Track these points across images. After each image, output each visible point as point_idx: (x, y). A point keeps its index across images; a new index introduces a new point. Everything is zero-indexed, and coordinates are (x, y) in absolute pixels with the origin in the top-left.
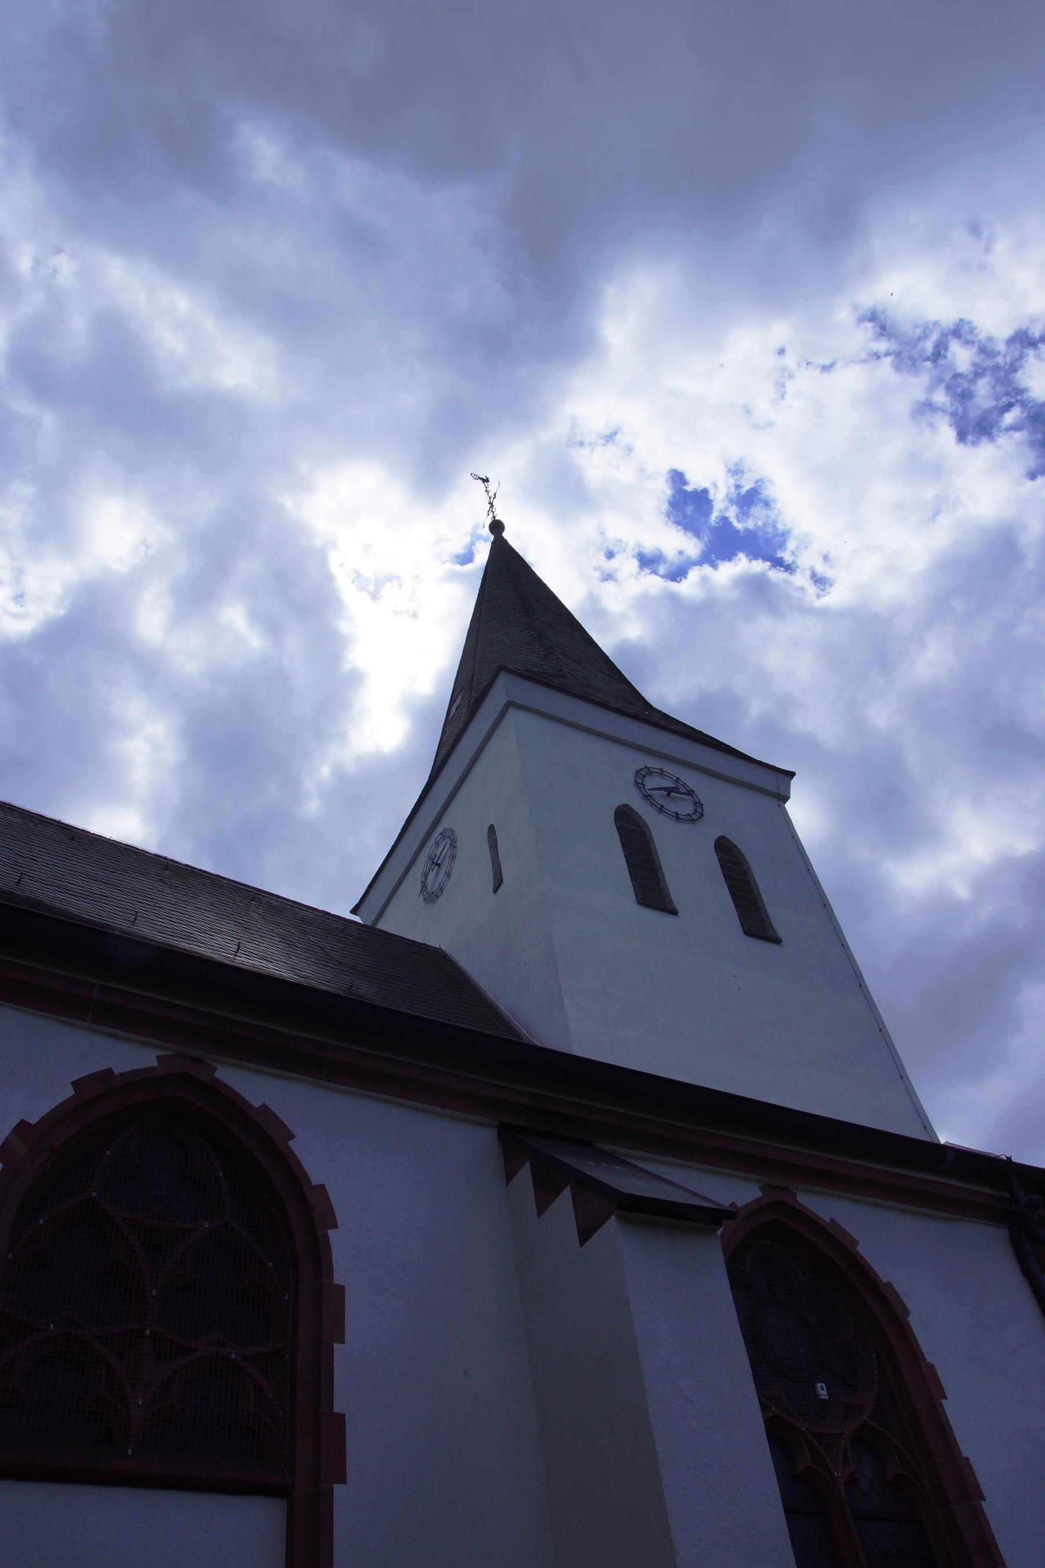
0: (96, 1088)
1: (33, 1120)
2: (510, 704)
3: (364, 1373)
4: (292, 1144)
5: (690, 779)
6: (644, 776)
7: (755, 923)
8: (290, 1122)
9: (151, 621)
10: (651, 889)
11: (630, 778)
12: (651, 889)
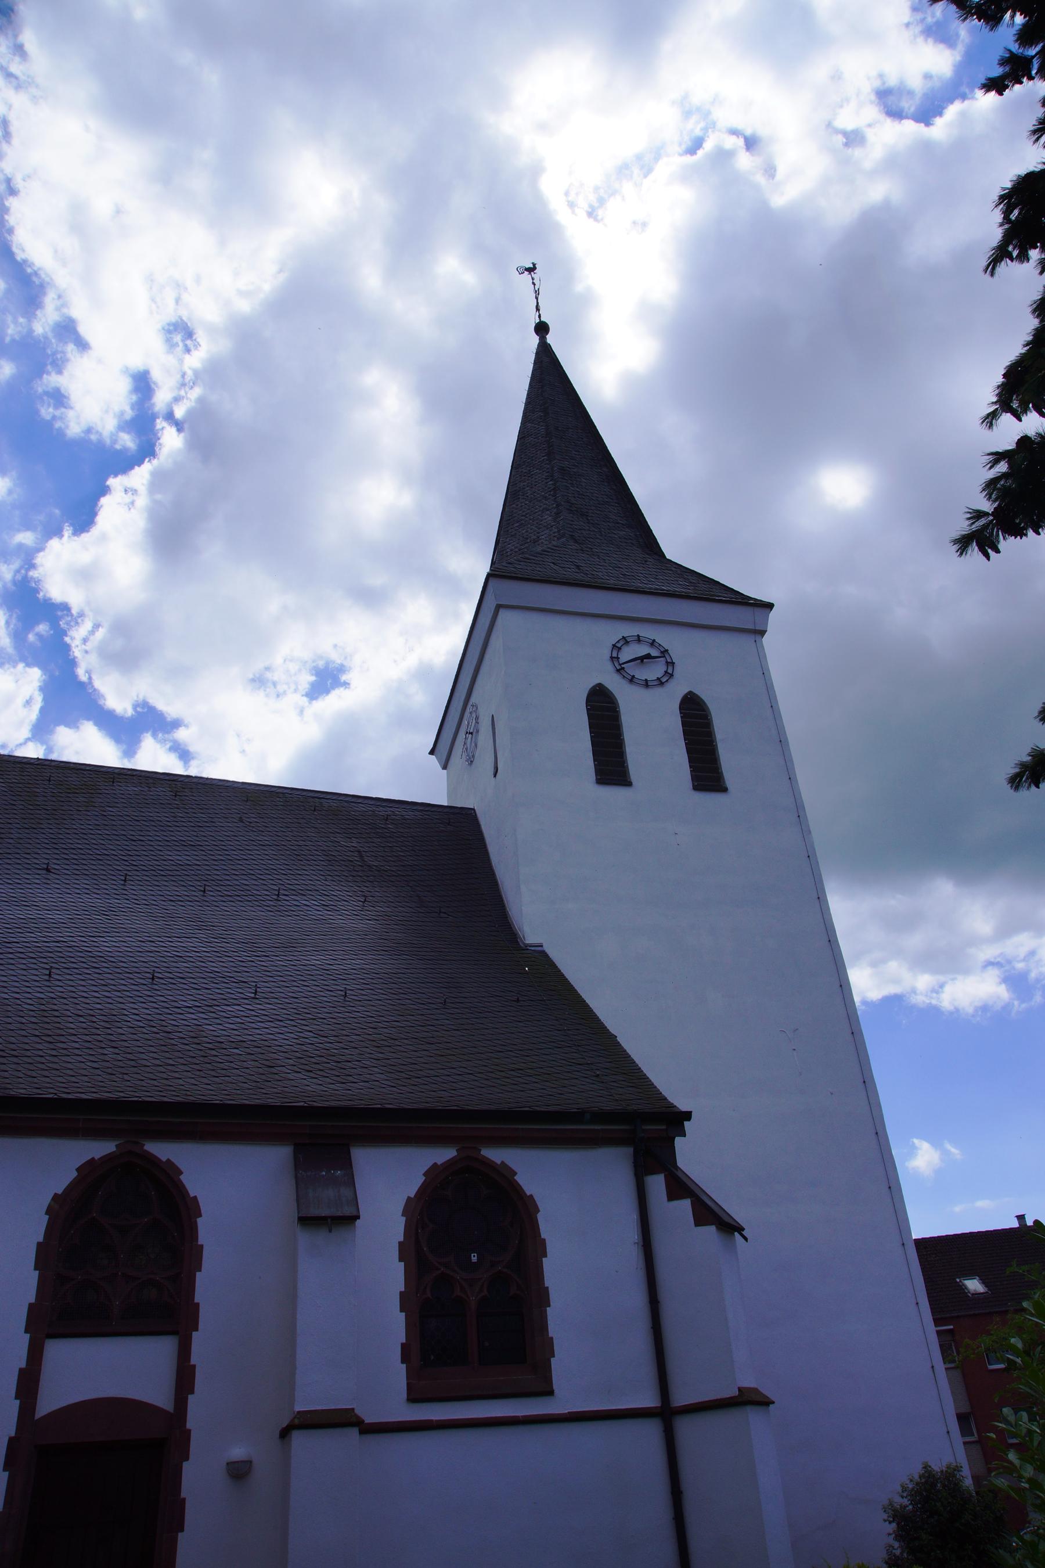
0: (88, 1169)
1: (60, 1192)
2: (499, 607)
3: (210, 1287)
4: (182, 1177)
5: (665, 637)
6: (620, 649)
7: (706, 773)
8: (182, 1168)
9: (371, 279)
10: (611, 766)
11: (606, 653)
12: (611, 766)
